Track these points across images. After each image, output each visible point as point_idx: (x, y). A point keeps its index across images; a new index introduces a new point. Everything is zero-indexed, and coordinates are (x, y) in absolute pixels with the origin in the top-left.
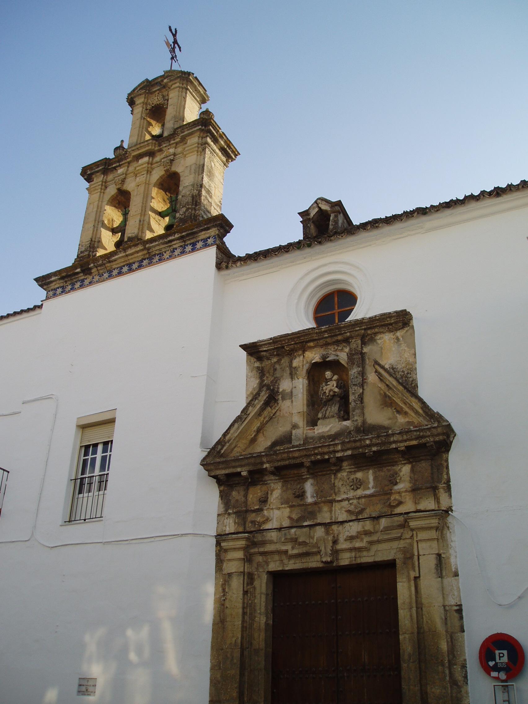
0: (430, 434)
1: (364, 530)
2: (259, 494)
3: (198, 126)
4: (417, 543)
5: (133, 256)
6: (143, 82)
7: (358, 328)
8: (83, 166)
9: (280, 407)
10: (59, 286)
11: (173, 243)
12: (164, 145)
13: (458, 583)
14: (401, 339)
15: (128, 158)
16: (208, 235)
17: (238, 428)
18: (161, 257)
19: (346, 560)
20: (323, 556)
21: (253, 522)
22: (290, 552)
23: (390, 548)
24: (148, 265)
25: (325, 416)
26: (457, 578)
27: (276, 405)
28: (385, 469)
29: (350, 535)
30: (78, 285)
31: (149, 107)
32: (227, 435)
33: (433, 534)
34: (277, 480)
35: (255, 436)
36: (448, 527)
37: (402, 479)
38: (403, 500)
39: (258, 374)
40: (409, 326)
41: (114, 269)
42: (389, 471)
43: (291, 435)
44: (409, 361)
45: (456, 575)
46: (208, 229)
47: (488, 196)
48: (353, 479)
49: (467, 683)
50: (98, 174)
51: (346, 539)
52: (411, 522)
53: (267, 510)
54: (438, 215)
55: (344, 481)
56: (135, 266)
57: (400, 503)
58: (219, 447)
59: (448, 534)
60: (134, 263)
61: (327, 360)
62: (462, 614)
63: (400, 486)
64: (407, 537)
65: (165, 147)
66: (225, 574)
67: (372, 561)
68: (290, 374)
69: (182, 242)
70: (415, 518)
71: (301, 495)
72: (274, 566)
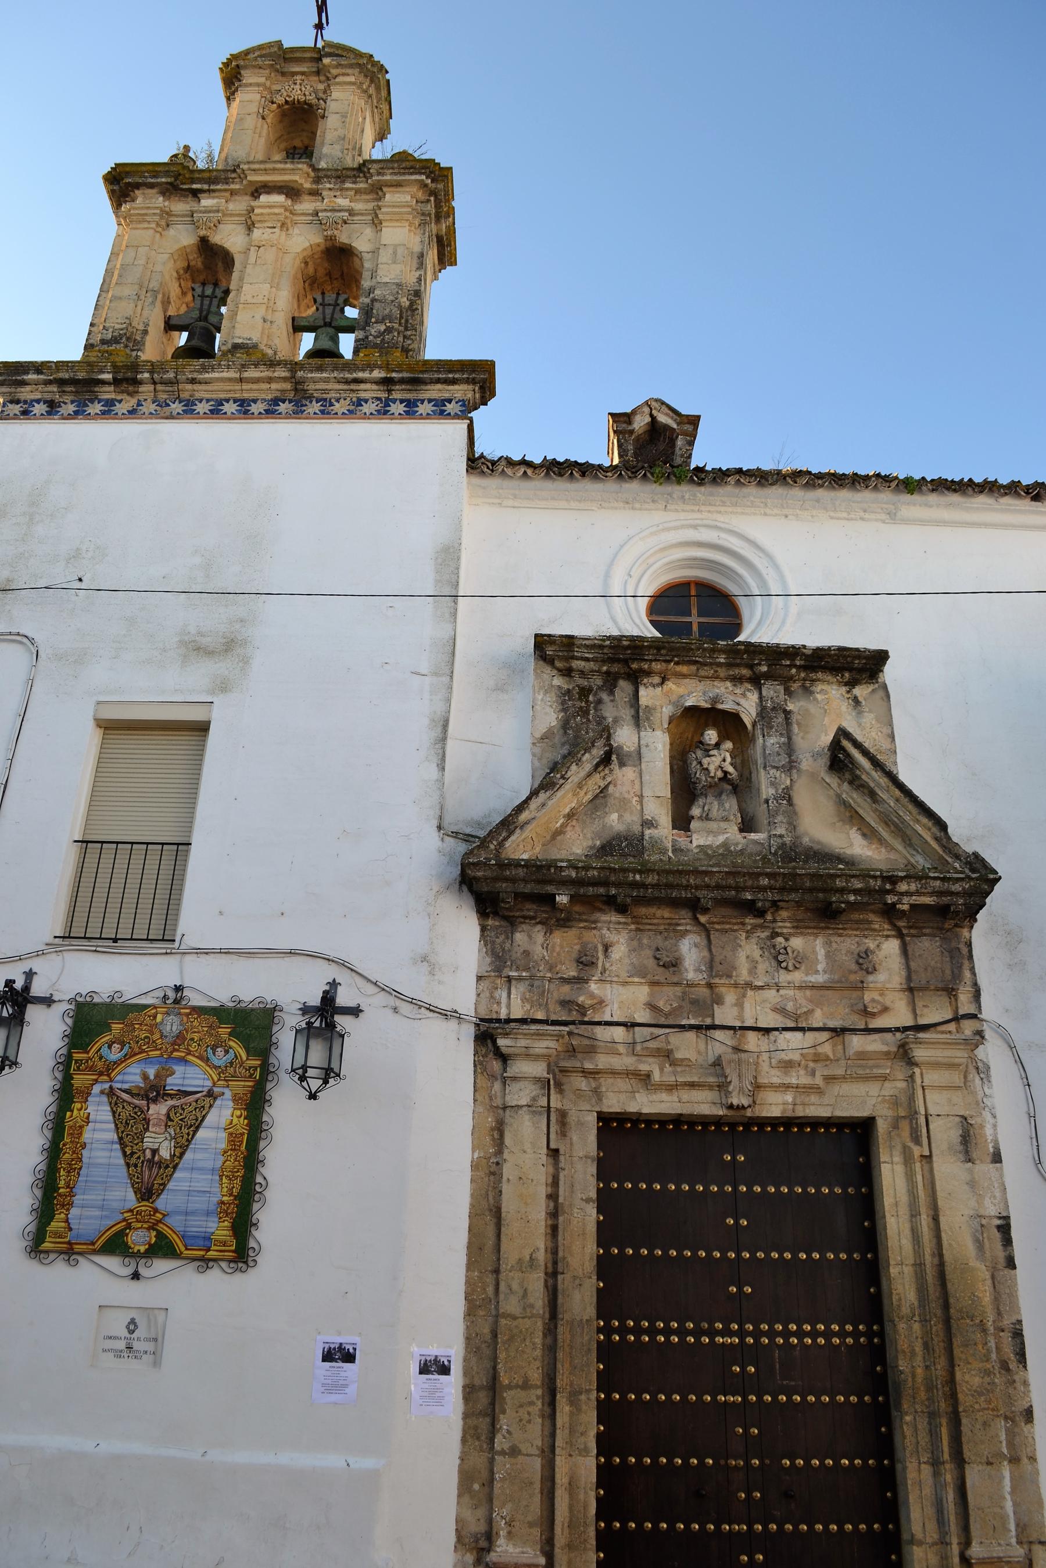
1: (815, 1053)
3: (421, 174)
4: (924, 1089)
5: (255, 386)
6: (270, 45)
8: (118, 162)
10: (40, 397)
11: (362, 386)
12: (328, 186)
13: (1002, 1176)
15: (233, 183)
16: (447, 395)
18: (325, 406)
22: (656, 1076)
24: (293, 415)
26: (998, 1165)
30: (96, 408)
31: (280, 100)
38: (888, 1003)
40: (877, 682)
41: (201, 401)
45: (997, 1158)
46: (454, 382)
47: (1023, 493)
49: (1025, 1367)
50: (154, 191)
52: (918, 1050)
54: (933, 498)
56: (255, 408)
57: (885, 1009)
60: (255, 401)
63: (880, 978)
65: (330, 189)
67: (829, 1115)
69: (384, 391)
72: (614, 1103)
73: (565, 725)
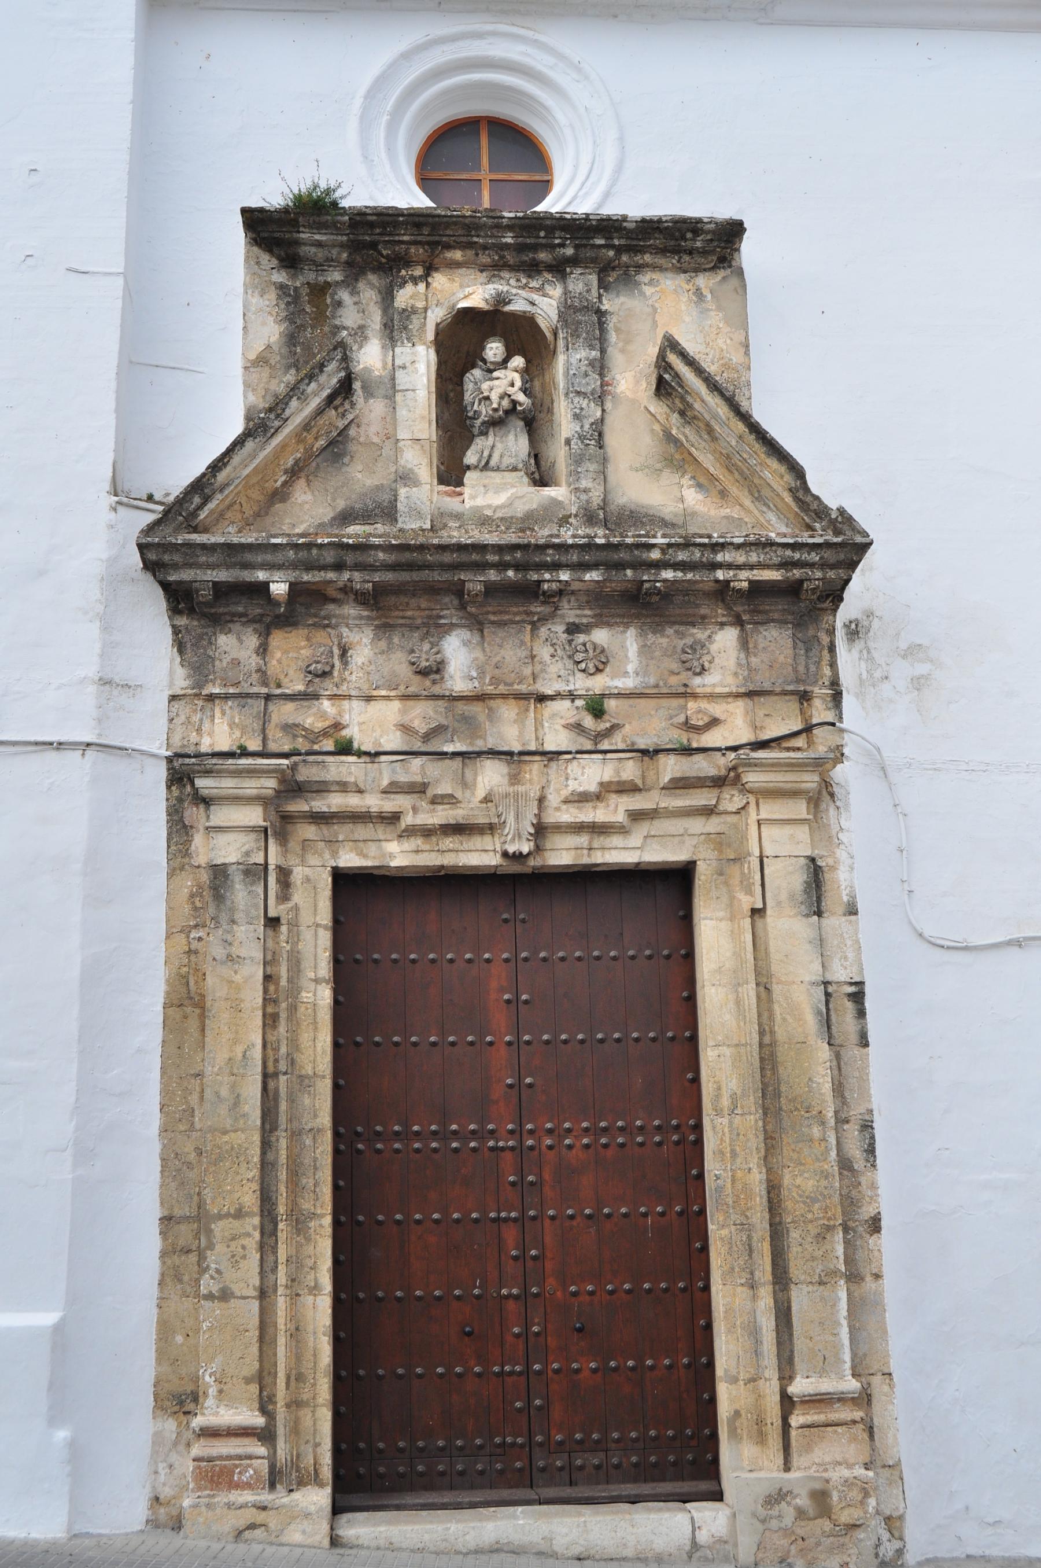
0: (818, 558)
2: (302, 652)
4: (759, 825)
7: (601, 242)
9: (357, 417)
14: (709, 296)
17: (253, 456)
19: (564, 852)
20: (510, 837)
21: (290, 728)
23: (681, 831)
25: (487, 463)
26: (853, 918)
27: (347, 406)
28: (670, 631)
29: (581, 789)
32: (220, 469)
33: (800, 809)
34: (361, 618)
35: (285, 484)
36: (832, 795)
37: (716, 660)
39: (283, 306)
40: (730, 266)
42: (681, 635)
43: (396, 500)
44: (731, 360)
45: (852, 910)
48: (584, 645)
49: (874, 1166)
51: (566, 798)
53: (333, 697)
55: (557, 647)
58: (197, 500)
59: (832, 811)
61: (508, 308)
62: (863, 1004)
64: (730, 809)
66: (198, 867)
68: (385, 325)
70: (762, 765)
71: (435, 671)
73: (291, 339)
